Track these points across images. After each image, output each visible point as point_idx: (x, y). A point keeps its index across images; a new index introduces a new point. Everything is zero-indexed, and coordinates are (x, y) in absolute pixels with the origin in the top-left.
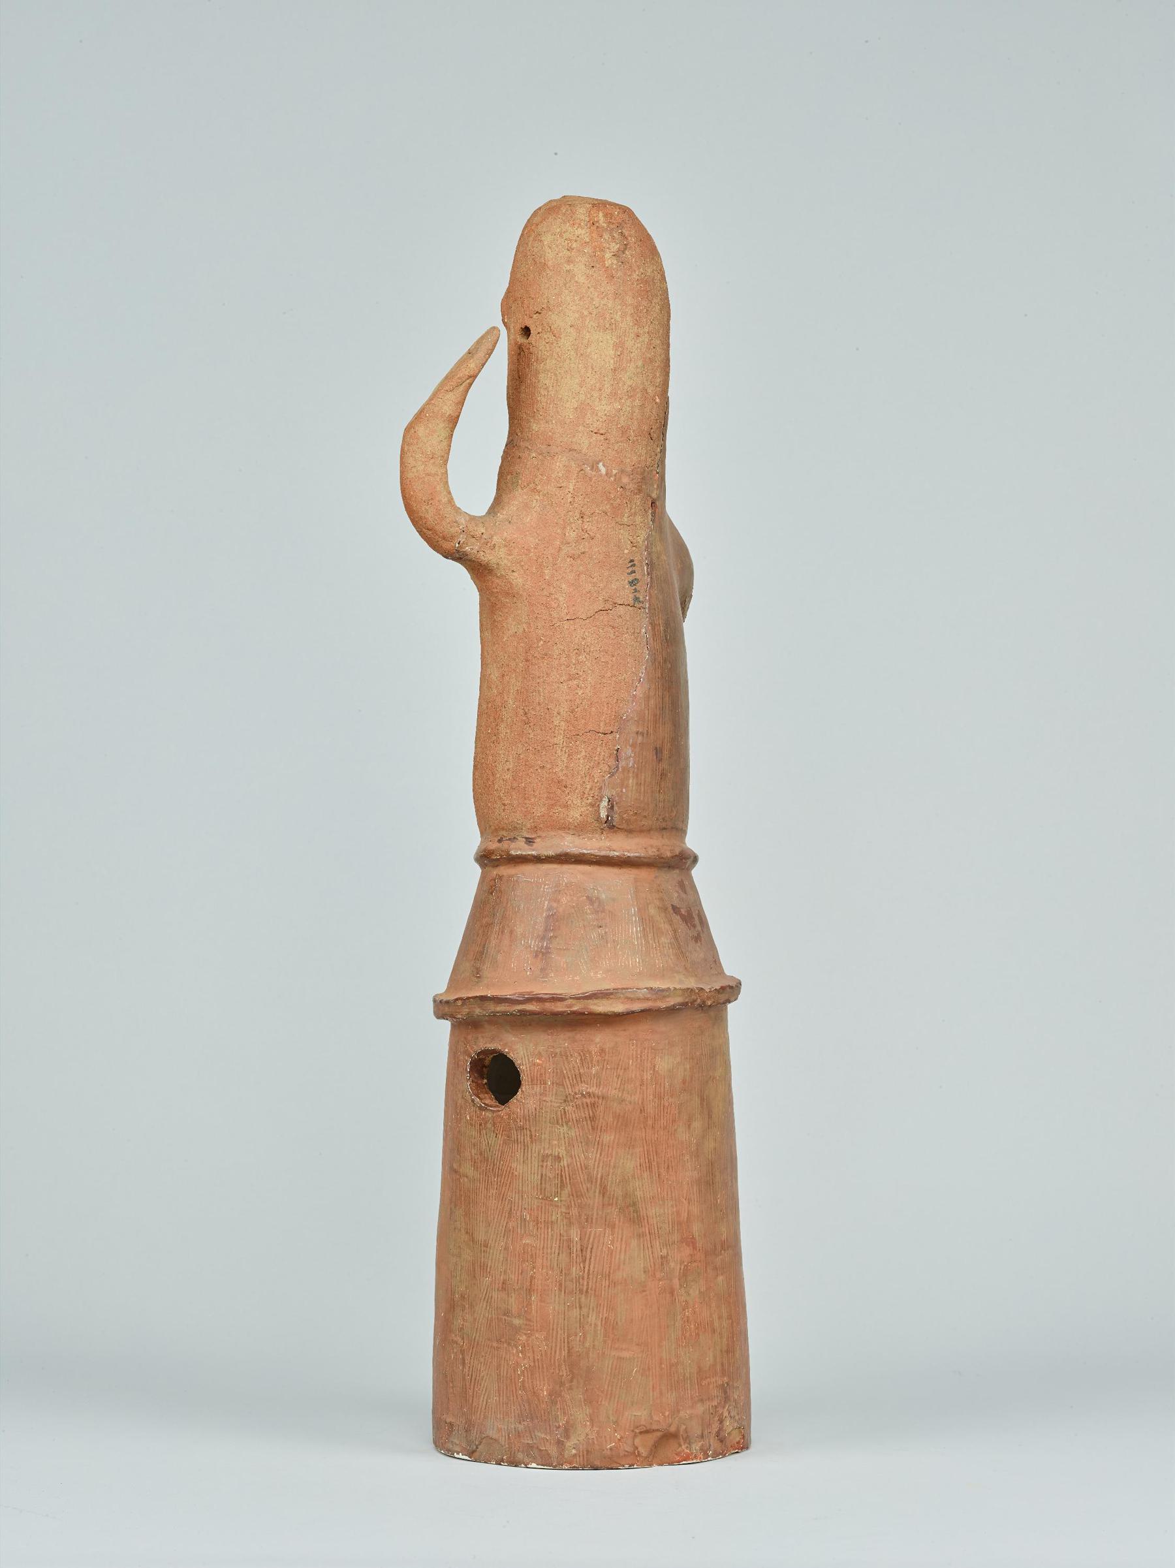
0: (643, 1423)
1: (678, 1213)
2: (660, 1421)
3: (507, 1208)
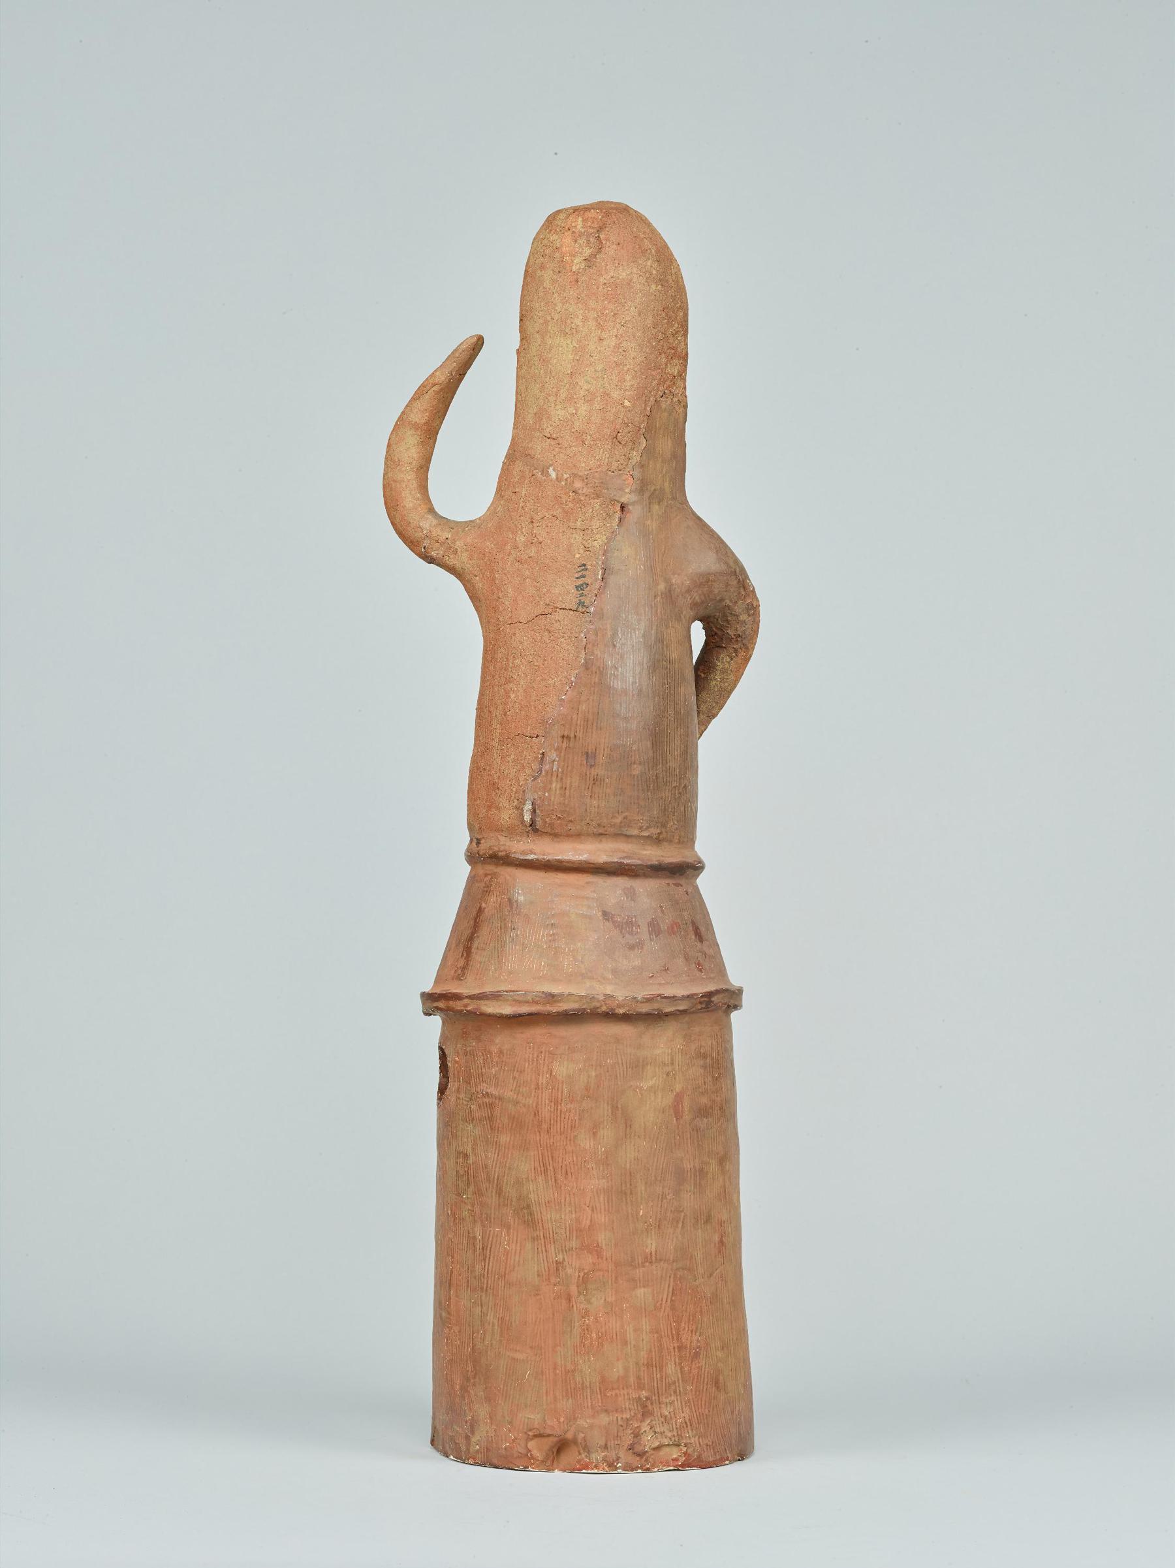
0: (536, 1426)
1: (578, 1220)
2: (555, 1426)
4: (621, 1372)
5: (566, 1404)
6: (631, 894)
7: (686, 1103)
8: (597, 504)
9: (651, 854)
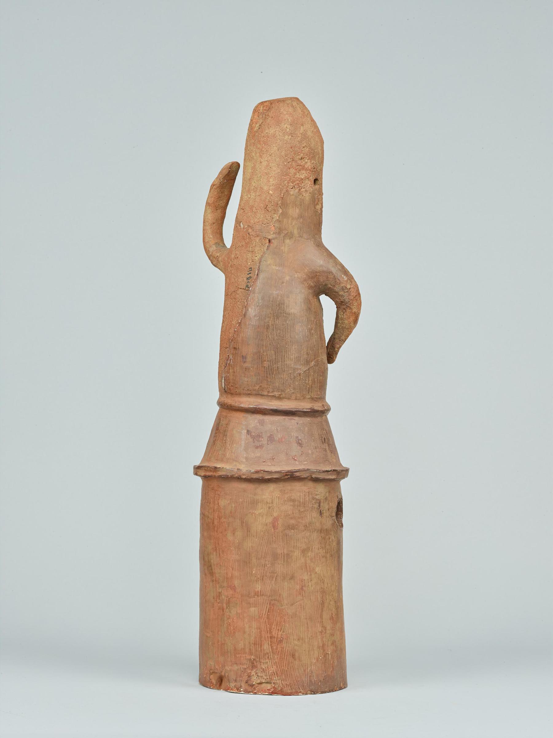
1: (227, 573)
4: (243, 647)
5: (221, 659)
6: (262, 423)
7: (280, 522)
8: (257, 239)
9: (306, 406)
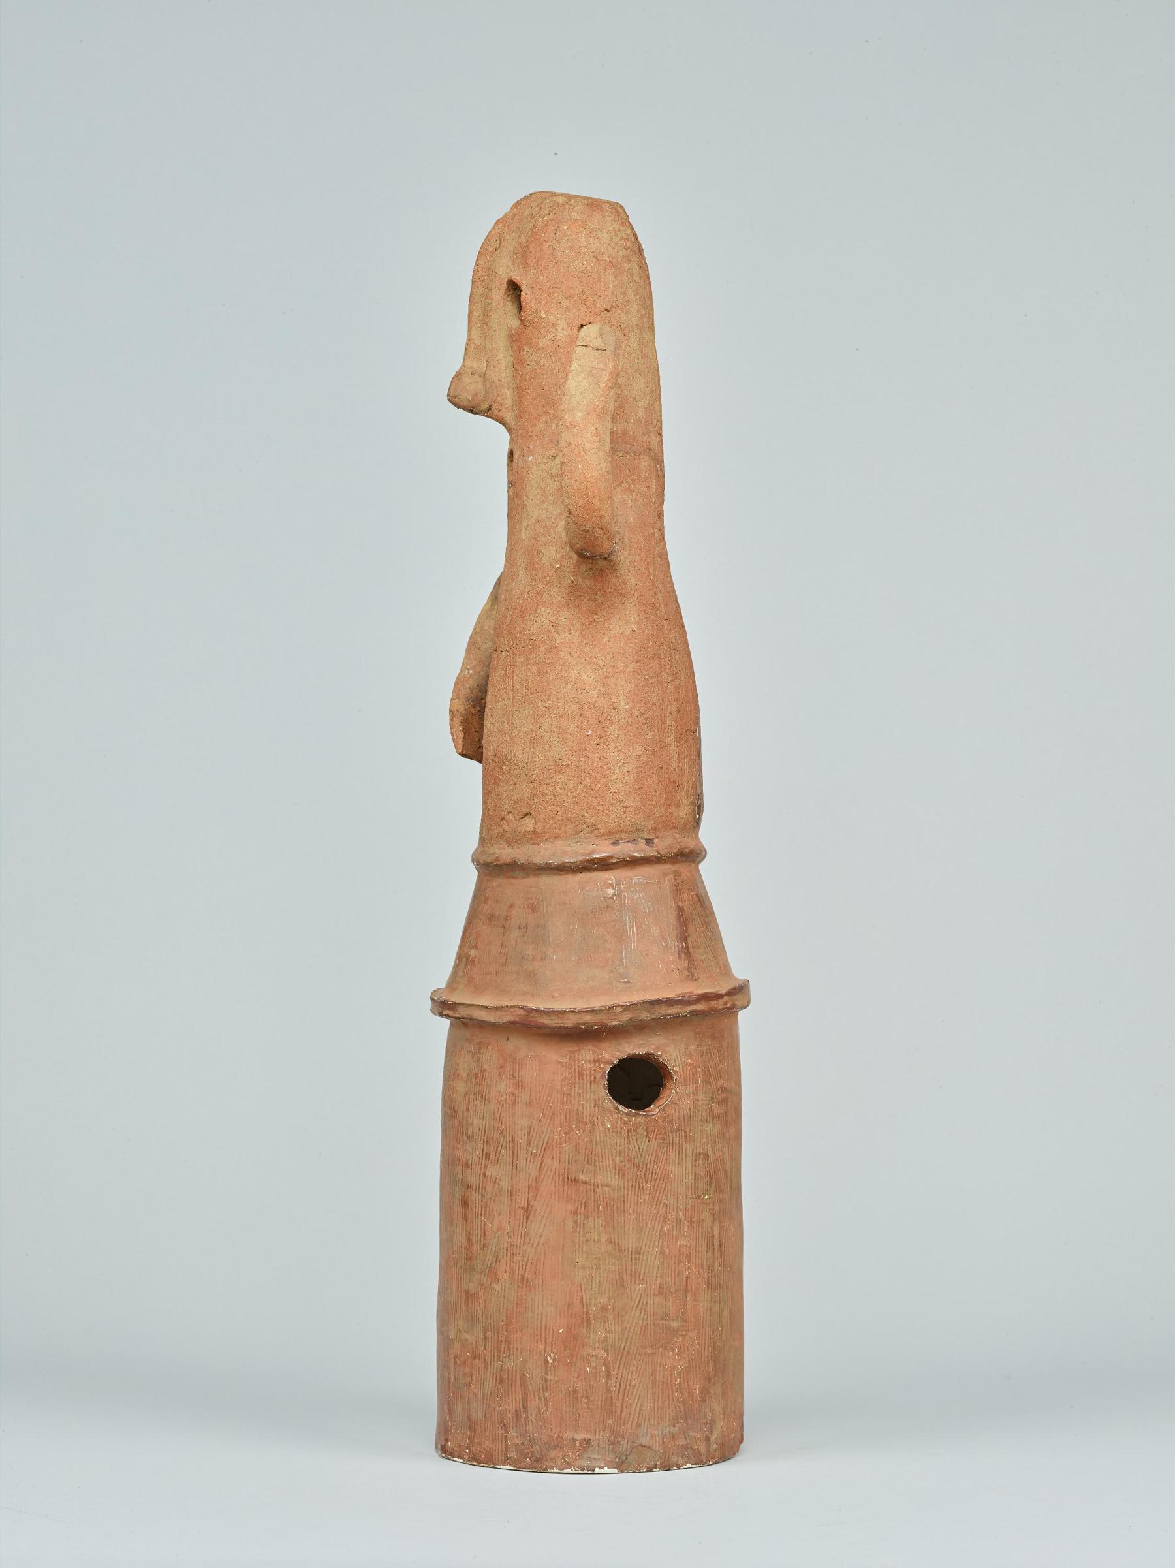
3: (662, 1211)
